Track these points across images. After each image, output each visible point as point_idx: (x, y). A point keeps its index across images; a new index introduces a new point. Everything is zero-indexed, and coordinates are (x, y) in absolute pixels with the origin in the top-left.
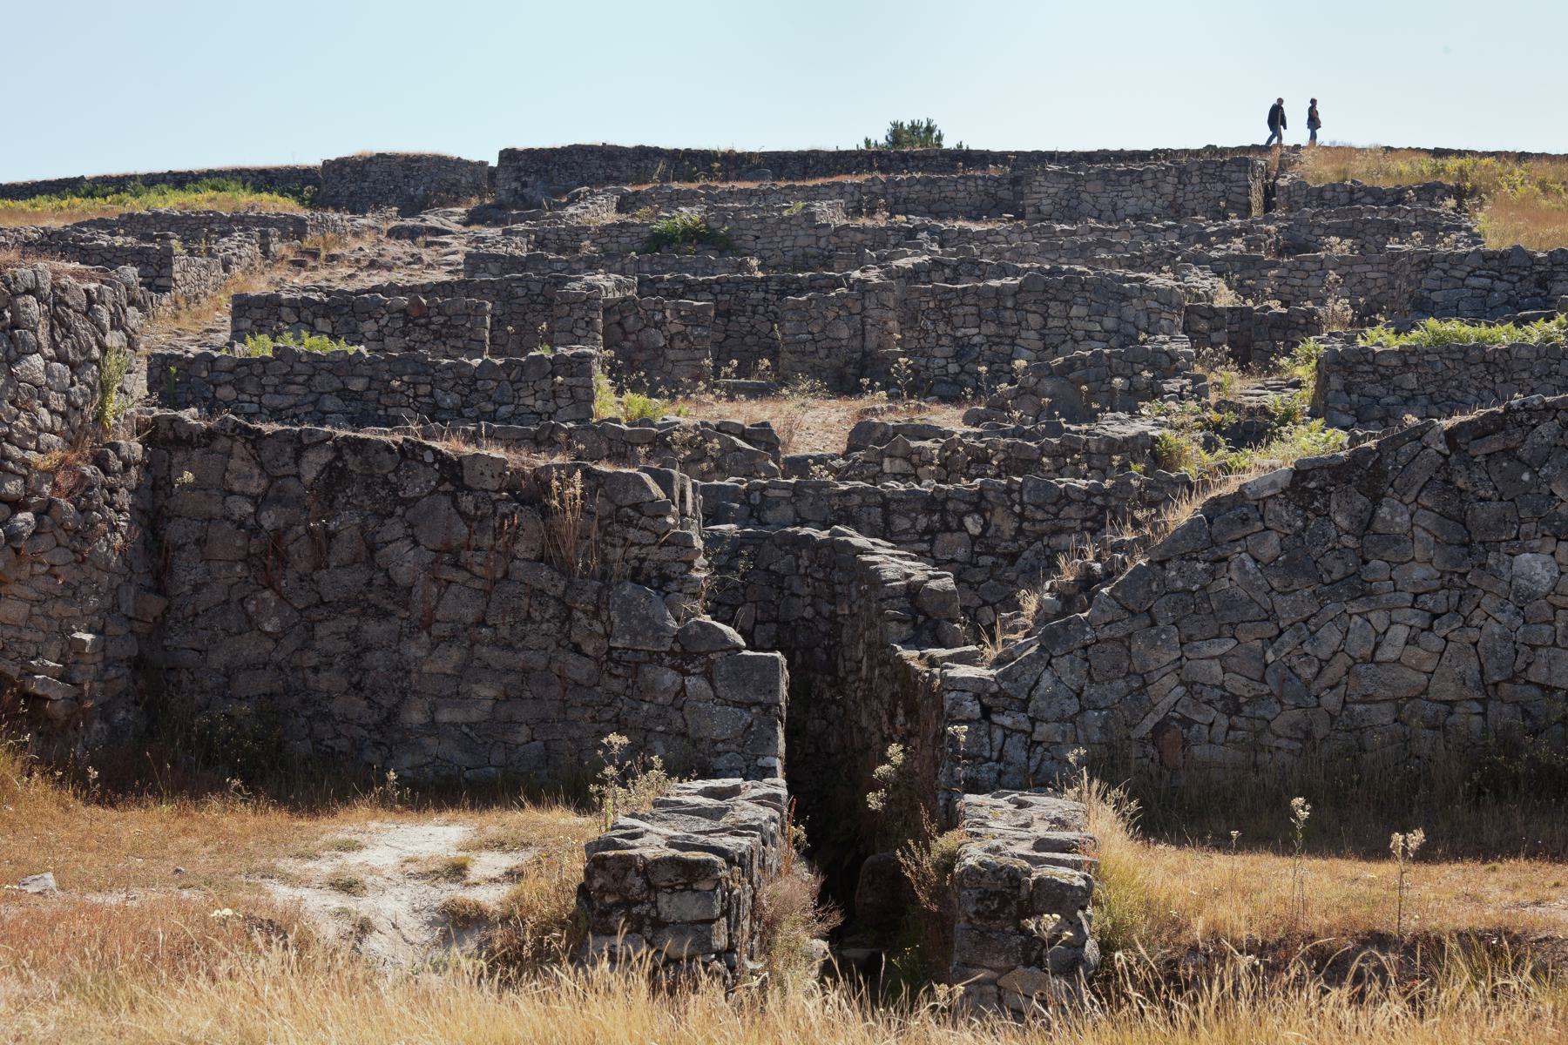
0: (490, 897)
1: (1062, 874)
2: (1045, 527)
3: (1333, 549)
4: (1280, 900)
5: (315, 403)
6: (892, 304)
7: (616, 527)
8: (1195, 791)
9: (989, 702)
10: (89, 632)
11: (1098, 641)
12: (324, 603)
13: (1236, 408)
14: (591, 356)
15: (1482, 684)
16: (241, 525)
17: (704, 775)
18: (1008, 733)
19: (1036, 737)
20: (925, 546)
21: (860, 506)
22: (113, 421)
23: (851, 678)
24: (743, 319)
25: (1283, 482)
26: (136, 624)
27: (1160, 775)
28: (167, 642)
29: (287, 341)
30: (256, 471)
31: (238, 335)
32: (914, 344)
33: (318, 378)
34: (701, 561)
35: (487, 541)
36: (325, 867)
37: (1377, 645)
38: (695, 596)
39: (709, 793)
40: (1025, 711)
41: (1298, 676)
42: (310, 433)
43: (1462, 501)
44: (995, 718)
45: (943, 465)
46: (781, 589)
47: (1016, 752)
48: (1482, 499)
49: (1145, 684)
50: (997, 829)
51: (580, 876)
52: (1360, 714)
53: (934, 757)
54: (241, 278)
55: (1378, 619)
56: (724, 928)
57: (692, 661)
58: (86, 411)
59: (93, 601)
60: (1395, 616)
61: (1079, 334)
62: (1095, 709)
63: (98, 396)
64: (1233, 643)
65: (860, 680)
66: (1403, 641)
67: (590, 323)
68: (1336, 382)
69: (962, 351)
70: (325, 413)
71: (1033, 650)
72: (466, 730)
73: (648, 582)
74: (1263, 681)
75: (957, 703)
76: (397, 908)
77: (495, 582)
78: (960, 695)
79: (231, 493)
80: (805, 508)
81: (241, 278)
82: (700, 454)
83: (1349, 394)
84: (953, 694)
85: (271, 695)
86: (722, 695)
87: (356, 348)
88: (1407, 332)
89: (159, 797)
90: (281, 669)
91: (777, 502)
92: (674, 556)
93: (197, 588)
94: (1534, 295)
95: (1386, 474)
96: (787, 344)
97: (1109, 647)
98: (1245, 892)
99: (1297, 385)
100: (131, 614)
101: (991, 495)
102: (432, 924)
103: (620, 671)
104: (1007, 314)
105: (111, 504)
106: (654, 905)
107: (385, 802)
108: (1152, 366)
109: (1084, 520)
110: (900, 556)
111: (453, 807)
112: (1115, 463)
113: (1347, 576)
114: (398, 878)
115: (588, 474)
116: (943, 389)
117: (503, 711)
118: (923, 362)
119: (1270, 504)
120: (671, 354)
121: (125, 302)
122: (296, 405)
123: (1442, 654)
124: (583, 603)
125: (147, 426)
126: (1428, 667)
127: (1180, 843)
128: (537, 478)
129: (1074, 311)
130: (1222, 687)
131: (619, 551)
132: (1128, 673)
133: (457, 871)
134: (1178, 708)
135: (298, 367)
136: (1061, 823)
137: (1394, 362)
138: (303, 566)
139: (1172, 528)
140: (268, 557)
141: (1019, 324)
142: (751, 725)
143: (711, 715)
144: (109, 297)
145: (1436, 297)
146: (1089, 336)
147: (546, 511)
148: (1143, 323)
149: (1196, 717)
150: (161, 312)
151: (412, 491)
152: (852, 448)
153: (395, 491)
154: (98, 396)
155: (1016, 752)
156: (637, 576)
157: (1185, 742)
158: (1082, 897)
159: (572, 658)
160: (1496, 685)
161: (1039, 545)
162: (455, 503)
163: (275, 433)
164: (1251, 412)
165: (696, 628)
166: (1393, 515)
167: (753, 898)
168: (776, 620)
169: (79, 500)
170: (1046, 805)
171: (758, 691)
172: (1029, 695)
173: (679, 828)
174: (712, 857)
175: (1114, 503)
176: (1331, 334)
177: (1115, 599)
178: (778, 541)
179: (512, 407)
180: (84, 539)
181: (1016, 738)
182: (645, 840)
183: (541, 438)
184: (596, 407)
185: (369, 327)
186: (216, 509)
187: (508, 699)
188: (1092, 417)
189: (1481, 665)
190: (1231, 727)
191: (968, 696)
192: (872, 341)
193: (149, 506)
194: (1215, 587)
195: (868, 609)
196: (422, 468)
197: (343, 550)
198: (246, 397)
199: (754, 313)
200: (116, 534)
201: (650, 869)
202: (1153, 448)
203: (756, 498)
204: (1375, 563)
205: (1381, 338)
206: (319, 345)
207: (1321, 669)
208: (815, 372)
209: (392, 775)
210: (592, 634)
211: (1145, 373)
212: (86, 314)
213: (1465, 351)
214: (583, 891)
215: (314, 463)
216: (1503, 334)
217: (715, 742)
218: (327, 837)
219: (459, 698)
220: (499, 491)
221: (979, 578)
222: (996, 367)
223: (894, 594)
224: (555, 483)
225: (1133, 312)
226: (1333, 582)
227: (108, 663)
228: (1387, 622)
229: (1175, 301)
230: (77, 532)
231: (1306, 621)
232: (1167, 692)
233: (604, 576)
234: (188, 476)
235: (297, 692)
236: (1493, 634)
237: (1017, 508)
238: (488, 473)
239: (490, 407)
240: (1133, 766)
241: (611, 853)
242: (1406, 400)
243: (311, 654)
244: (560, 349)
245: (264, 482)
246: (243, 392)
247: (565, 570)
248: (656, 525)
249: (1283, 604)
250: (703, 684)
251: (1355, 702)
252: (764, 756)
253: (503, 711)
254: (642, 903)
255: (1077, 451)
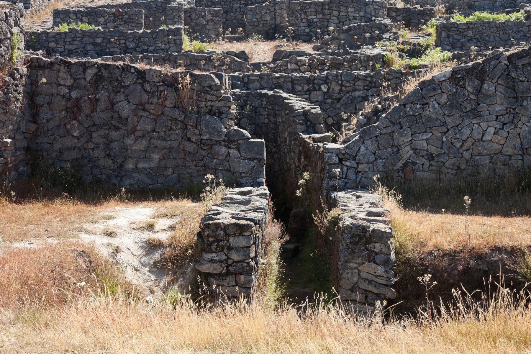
0: (164, 237)
1: (381, 227)
2: (350, 89)
3: (467, 99)
4: (460, 233)
5: (84, 47)
6: (285, 8)
7: (203, 94)
8: (418, 189)
9: (341, 157)
10: (9, 138)
11: (381, 134)
12: (95, 125)
13: (410, 44)
14: (181, 29)
15: (522, 149)
16: (64, 97)
17: (239, 185)
18: (349, 168)
19: (359, 169)
20: (307, 96)
21: (284, 82)
22: (16, 60)
23: (283, 145)
24: (232, 14)
25: (448, 75)
26: (26, 134)
27: (405, 183)
28: (37, 141)
29: (73, 26)
30: (69, 77)
31: (55, 24)
32: (293, 22)
33: (85, 39)
34: (233, 106)
35: (155, 100)
36: (101, 226)
37: (483, 135)
38: (232, 119)
39: (241, 193)
40: (355, 160)
41: (455, 146)
42: (89, 62)
43: (514, 82)
44: (344, 163)
45: (309, 66)
46: (256, 112)
47: (352, 175)
48: (521, 81)
49: (399, 150)
50: (353, 207)
51: (199, 230)
52: (477, 160)
53: (321, 177)
54: (54, 3)
55: (484, 125)
56: (254, 249)
57: (232, 143)
58: (6, 56)
59: (10, 127)
60: (490, 124)
61: (351, 18)
62: (381, 159)
63: (10, 51)
64: (431, 134)
65: (286, 145)
66: (492, 133)
67: (179, 16)
68: (444, 34)
69: (310, 24)
70: (87, 51)
71: (357, 137)
72: (149, 170)
73: (214, 114)
74: (442, 148)
75: (330, 158)
76: (130, 244)
77: (158, 116)
78: (331, 154)
79: (60, 85)
80: (264, 84)
81: (54, 3)
82: (223, 64)
83: (448, 38)
84: (328, 154)
85: (77, 159)
86: (243, 156)
87: (98, 27)
88: (468, 16)
89: (38, 200)
90: (80, 149)
91: (254, 81)
92: (224, 105)
93: (48, 121)
94: (510, 3)
95: (486, 72)
96: (248, 23)
97: (385, 136)
98: (447, 231)
99: (429, 35)
100: (24, 131)
101: (330, 78)
102: (142, 247)
103: (205, 148)
104: (326, 11)
105: (16, 91)
106: (228, 241)
107: (121, 199)
108: (379, 29)
109: (364, 86)
110: (299, 100)
111: (146, 201)
112: (370, 64)
113: (472, 110)
114: (129, 230)
115: (192, 75)
116: (304, 38)
117: (163, 163)
118: (296, 28)
119: (444, 83)
120: (208, 27)
121: (19, 16)
122: (77, 48)
123: (507, 138)
124: (191, 123)
125: (28, 62)
126: (502, 143)
127: (417, 210)
128: (173, 77)
129: (350, 10)
130: (427, 150)
131: (204, 103)
132: (392, 146)
133: (151, 227)
134: (411, 158)
135: (77, 35)
136: (373, 204)
137: (464, 27)
138: (87, 111)
139: (407, 92)
140: (74, 109)
141: (330, 14)
142: (254, 167)
143: (239, 163)
144: (13, 14)
145: (476, 4)
146: (355, 18)
147: (177, 89)
148: (373, 13)
149: (418, 162)
150: (27, 16)
151: (127, 83)
152: (274, 60)
153: (120, 83)
154: (10, 51)
155: (352, 175)
156: (210, 112)
157: (414, 171)
158: (389, 236)
159: (187, 143)
160: (527, 149)
161: (348, 95)
162: (143, 87)
163: (76, 63)
164: (414, 45)
165: (233, 131)
166: (488, 87)
167: (262, 235)
168: (254, 124)
169: (4, 90)
170: (367, 197)
171: (256, 154)
172: (356, 154)
173: (234, 209)
174: (249, 222)
175: (375, 80)
176: (440, 17)
177: (387, 118)
178: (255, 95)
179: (154, 47)
180: (7, 104)
181: (351, 170)
182: (223, 214)
183: (166, 59)
184: (183, 46)
185: (101, 20)
186: (55, 91)
187: (164, 158)
188: (359, 47)
189: (521, 142)
190: (430, 165)
191: (334, 155)
192: (278, 21)
193: (30, 91)
194: (424, 114)
195: (289, 120)
196: (130, 74)
197: (102, 105)
198: (59, 46)
199: (236, 12)
200: (18, 102)
201: (226, 228)
202: (383, 59)
203: (246, 80)
204: (482, 105)
205: (458, 18)
206: (84, 27)
207: (463, 143)
208: (258, 32)
209: (123, 189)
210: (195, 134)
211: (377, 32)
212: (5, 21)
213: (489, 23)
214: (199, 234)
215: (90, 74)
216: (502, 17)
217: (241, 173)
218: (101, 214)
219: (147, 159)
220: (159, 82)
221: (327, 107)
222: (322, 29)
223: (299, 115)
224: (180, 79)
225: (370, 10)
226: (467, 112)
227: (16, 149)
228: (487, 126)
229: (384, 6)
230: (4, 102)
231: (457, 126)
232: (407, 152)
233: (198, 113)
234: (44, 80)
235: (86, 158)
236: (526, 130)
237: (340, 82)
238: (155, 76)
239: (146, 47)
240: (395, 180)
241: (211, 222)
242: (469, 40)
243: (91, 144)
244: (170, 26)
245: (72, 81)
246: (58, 44)
247: (184, 110)
248: (217, 93)
249: (449, 120)
250: (236, 152)
251: (475, 156)
252: (259, 178)
253: (163, 163)
254: (223, 240)
255: (356, 60)
